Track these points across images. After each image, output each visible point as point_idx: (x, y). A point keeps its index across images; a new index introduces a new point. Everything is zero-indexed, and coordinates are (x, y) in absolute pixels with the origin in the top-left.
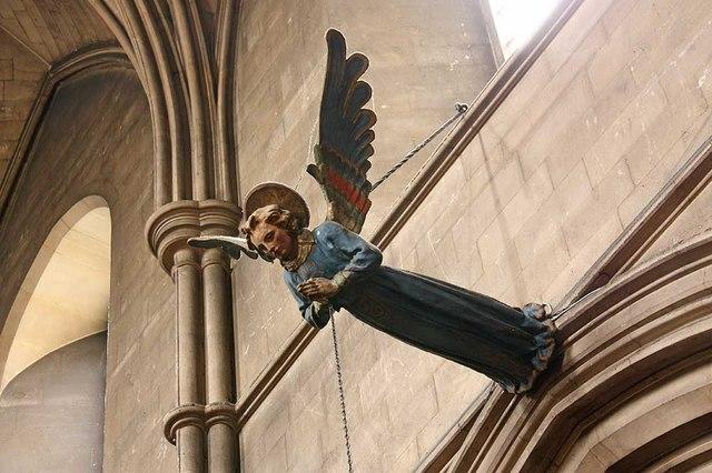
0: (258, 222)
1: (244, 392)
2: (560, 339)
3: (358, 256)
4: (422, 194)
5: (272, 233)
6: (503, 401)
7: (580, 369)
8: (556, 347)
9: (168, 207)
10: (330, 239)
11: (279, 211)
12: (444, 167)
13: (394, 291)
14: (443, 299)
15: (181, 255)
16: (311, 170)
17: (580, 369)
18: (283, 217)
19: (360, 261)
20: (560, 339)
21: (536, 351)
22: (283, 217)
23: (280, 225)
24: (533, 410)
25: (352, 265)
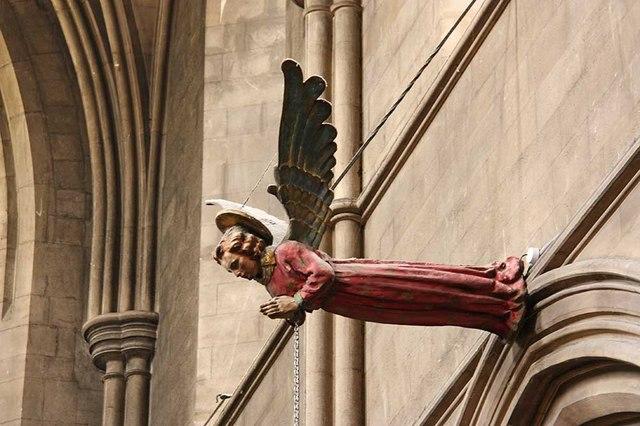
0: (223, 253)
1: (369, 178)
2: (532, 303)
3: (311, 279)
4: (415, 141)
5: (237, 261)
6: (497, 349)
7: (546, 340)
8: (526, 315)
9: (106, 315)
10: (288, 262)
11: (242, 238)
12: (487, 28)
13: (505, 74)
14: (401, 291)
15: (112, 367)
16: (272, 190)
17: (546, 340)
18: (245, 246)
19: (313, 284)
20: (532, 303)
21: (508, 315)
22: (245, 246)
23: (244, 253)
24: (520, 360)
25: (306, 287)
